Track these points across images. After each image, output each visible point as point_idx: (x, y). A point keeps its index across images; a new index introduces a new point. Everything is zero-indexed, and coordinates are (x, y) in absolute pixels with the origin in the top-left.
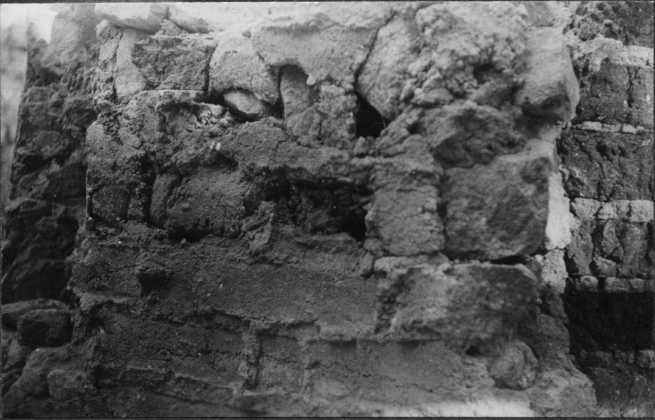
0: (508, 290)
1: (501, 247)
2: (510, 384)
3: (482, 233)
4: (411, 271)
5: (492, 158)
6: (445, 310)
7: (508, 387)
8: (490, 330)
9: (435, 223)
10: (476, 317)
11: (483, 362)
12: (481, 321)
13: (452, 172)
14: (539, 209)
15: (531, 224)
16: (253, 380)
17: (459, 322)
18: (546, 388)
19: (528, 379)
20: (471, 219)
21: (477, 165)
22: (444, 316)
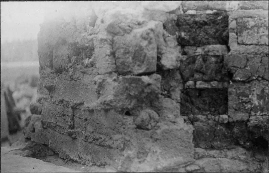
0: (136, 87)
1: (138, 69)
2: (143, 127)
3: (131, 63)
4: (104, 80)
5: (131, 31)
6: (113, 96)
7: (142, 129)
8: (132, 104)
9: (110, 60)
10: (126, 99)
11: (132, 118)
12: (128, 101)
13: (116, 38)
14: (149, 51)
15: (146, 58)
16: (72, 125)
17: (119, 101)
18: (157, 129)
19: (151, 125)
20: (126, 58)
21: (126, 35)
22: (112, 98)
